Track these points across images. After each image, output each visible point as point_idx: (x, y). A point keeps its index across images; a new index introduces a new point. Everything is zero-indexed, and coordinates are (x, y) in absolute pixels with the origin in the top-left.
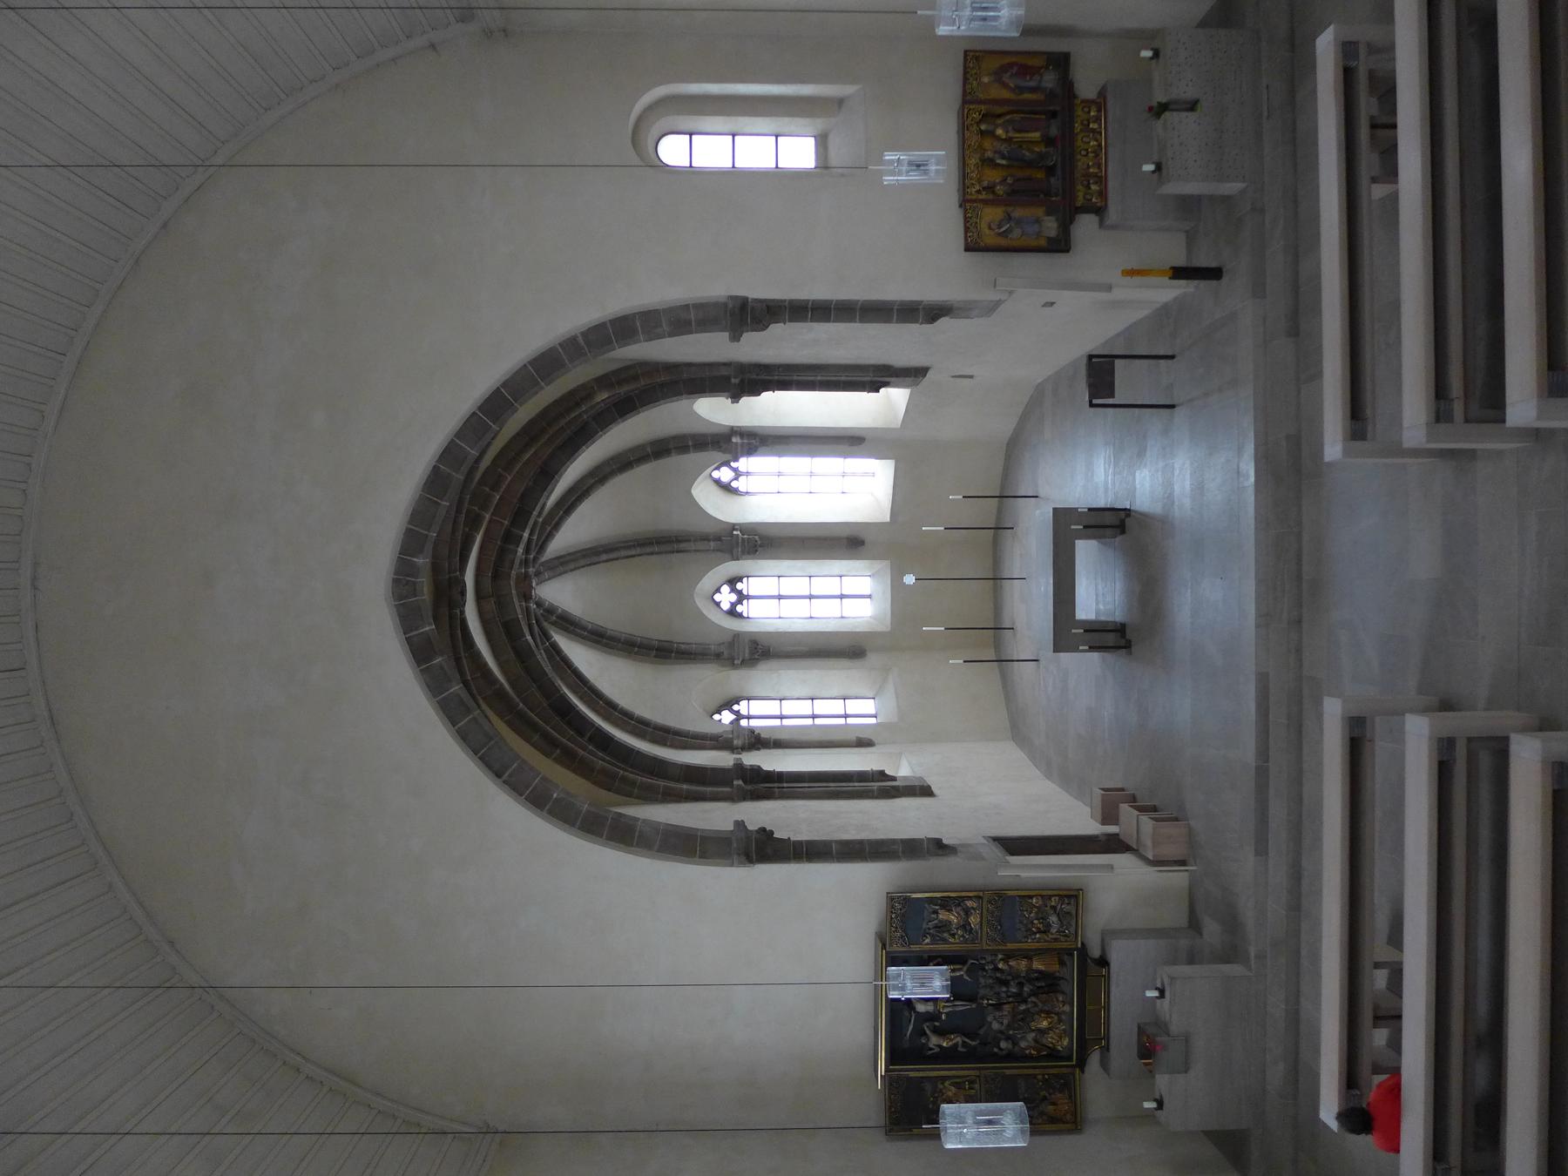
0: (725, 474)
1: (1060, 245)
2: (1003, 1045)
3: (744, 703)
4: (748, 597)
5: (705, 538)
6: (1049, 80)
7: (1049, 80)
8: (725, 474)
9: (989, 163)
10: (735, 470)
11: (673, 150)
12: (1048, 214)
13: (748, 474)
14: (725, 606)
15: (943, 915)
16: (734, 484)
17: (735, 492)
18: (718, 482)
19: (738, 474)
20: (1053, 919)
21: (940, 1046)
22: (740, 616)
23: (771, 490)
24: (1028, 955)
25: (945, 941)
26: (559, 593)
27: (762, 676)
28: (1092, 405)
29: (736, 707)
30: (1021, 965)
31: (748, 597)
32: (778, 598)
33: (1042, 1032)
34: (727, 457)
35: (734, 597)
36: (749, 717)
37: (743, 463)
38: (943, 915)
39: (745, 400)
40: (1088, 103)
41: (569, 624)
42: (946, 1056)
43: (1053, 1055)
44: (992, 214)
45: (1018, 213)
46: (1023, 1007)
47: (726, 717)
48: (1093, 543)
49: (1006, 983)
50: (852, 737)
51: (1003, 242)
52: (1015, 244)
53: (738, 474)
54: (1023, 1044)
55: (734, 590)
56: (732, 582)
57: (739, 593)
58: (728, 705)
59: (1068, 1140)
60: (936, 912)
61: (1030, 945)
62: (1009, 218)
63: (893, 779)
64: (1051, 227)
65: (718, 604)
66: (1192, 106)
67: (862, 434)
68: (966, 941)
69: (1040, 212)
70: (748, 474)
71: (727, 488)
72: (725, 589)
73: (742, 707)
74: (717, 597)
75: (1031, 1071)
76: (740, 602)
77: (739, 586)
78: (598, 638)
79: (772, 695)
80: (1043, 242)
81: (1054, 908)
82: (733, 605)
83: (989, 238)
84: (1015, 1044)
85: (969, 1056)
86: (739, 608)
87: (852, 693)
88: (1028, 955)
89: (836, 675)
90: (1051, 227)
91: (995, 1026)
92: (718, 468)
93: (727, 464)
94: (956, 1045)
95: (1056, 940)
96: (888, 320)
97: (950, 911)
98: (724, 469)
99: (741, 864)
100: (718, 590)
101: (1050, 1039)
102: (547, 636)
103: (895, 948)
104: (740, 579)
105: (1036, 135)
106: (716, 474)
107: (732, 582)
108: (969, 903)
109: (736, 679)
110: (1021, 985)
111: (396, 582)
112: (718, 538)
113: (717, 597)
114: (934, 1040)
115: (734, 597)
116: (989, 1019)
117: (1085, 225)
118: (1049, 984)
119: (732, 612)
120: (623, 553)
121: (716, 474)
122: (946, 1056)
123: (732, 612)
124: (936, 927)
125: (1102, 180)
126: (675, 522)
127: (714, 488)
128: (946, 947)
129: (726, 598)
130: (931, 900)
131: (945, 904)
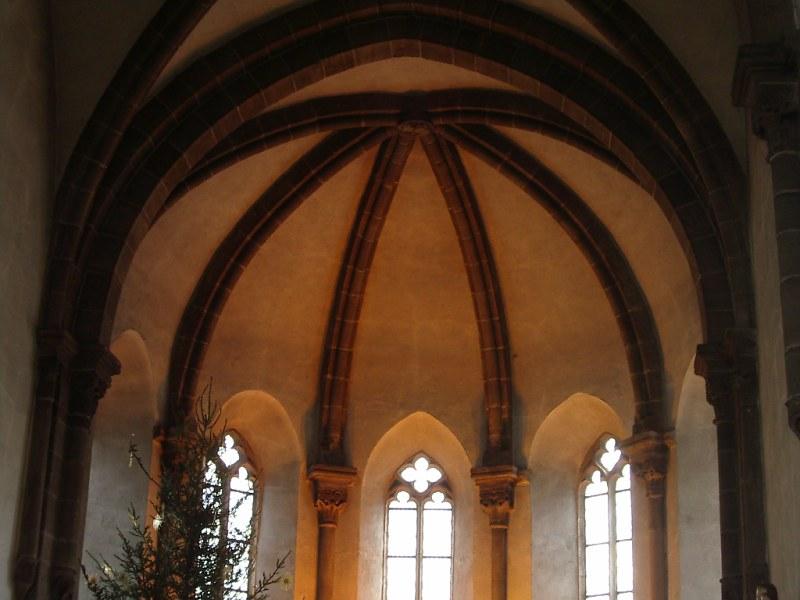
0: (611, 456)
4: (420, 510)
8: (611, 456)
14: (407, 475)
16: (596, 475)
17: (584, 477)
19: (611, 477)
26: (418, 212)
29: (243, 472)
31: (420, 510)
35: (421, 487)
39: (720, 585)
41: (373, 204)
48: (403, 177)
55: (433, 487)
56: (445, 485)
64: (713, 398)
65: (410, 461)
71: (591, 459)
72: (436, 475)
74: (422, 463)
77: (438, 497)
78: (357, 253)
86: (403, 496)
93: (625, 458)
100: (433, 462)
102: (322, 124)
104: (449, 497)
107: (445, 485)
113: (422, 463)
115: (421, 487)
123: (395, 485)
126: (528, 380)
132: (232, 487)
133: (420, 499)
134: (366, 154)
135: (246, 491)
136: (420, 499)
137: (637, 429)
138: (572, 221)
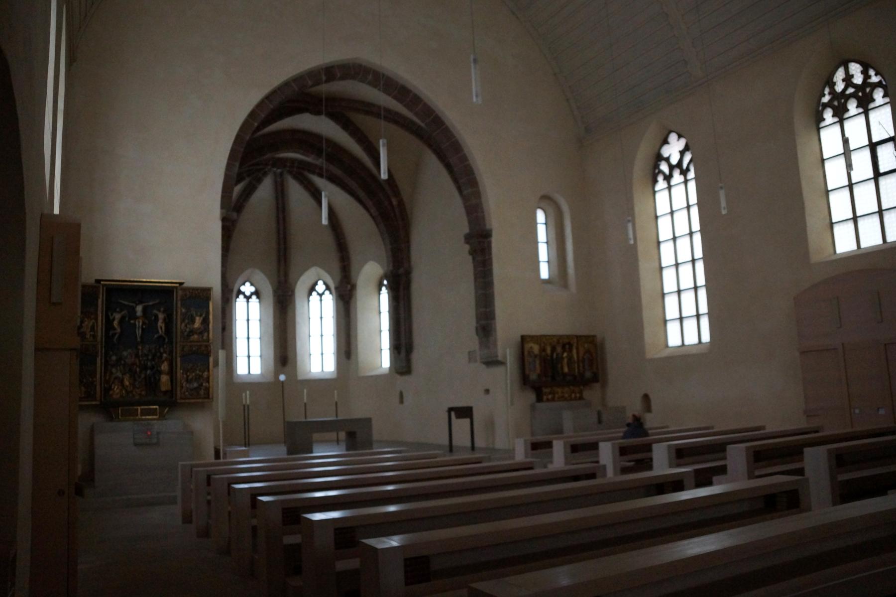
0: (320, 287)
1: (525, 380)
2: (114, 358)
4: (248, 302)
5: (286, 275)
6: (588, 374)
7: (588, 374)
8: (320, 287)
9: (554, 349)
10: (323, 293)
11: (541, 216)
12: (539, 376)
14: (243, 288)
15: (198, 321)
16: (314, 293)
17: (310, 294)
18: (316, 284)
20: (195, 385)
21: (114, 319)
22: (237, 297)
23: (318, 313)
24: (171, 373)
25: (183, 321)
28: (450, 410)
30: (165, 367)
31: (248, 302)
32: (318, 313)
33: (122, 382)
34: (332, 286)
35: (248, 294)
37: (329, 300)
38: (198, 321)
40: (581, 392)
42: (109, 322)
43: (107, 390)
44: (536, 349)
45: (538, 362)
46: (138, 370)
49: (153, 359)
51: (526, 353)
52: (526, 358)
53: (321, 295)
54: (114, 370)
55: (252, 294)
56: (257, 293)
57: (250, 297)
60: (201, 316)
61: (180, 372)
62: (536, 356)
64: (349, 286)
65: (244, 284)
66: (600, 422)
67: (353, 357)
68: (182, 332)
69: (538, 371)
71: (312, 289)
72: (253, 289)
74: (248, 284)
75: (98, 376)
76: (245, 297)
77: (254, 297)
80: (527, 372)
81: (201, 385)
82: (243, 293)
83: (528, 346)
84: (113, 366)
85: (108, 337)
86: (241, 296)
88: (171, 373)
90: (533, 376)
91: (125, 353)
92: (325, 283)
94: (115, 329)
95: (182, 387)
96: (478, 305)
97: (202, 323)
98: (324, 287)
99: (222, 214)
100: (252, 284)
101: (116, 388)
103: (180, 293)
104: (258, 297)
105: (566, 370)
106: (320, 283)
107: (257, 293)
108: (206, 334)
110: (152, 368)
111: (360, 66)
112: (286, 281)
113: (248, 284)
114: (118, 316)
115: (248, 294)
116: (130, 351)
117: (532, 397)
118: (152, 384)
119: (240, 292)
120: (281, 216)
121: (320, 283)
122: (109, 322)
124: (192, 316)
125: (553, 400)
126: (355, 258)
128: (179, 323)
129: (248, 289)
130: (208, 313)
131: (206, 321)
132: (320, 370)
133: (248, 298)
134: (406, 536)
135: (454, 443)
136: (248, 298)
138: (189, 403)
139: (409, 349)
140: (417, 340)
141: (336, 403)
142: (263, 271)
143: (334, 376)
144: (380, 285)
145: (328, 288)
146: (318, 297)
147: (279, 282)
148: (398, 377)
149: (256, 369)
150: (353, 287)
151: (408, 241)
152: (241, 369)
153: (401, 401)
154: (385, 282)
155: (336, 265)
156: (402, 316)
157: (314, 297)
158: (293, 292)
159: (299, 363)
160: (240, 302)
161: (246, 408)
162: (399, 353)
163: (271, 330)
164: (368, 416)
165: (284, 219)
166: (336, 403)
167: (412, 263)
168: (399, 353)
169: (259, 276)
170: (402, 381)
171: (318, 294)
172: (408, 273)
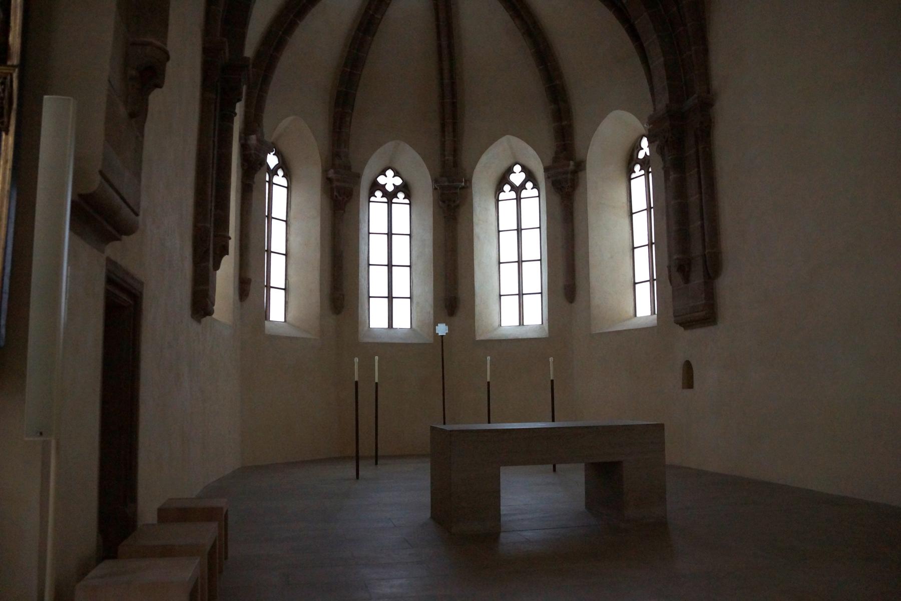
0: (518, 177)
3: (284, 182)
4: (390, 203)
5: (456, 152)
8: (518, 177)
10: (523, 186)
13: (518, 199)
14: (381, 180)
16: (507, 188)
17: (500, 189)
18: (510, 171)
19: (518, 190)
23: (514, 231)
27: (312, 198)
31: (390, 203)
32: (514, 231)
35: (390, 188)
36: (271, 183)
37: (533, 206)
47: (272, 160)
50: (252, 275)
53: (518, 190)
55: (397, 189)
56: (405, 188)
58: (283, 164)
59: (712, 328)
63: (217, 266)
65: (383, 173)
70: (518, 199)
71: (504, 179)
72: (398, 181)
73: (280, 179)
74: (390, 173)
76: (385, 194)
77: (401, 195)
79: (292, 214)
82: (382, 188)
86: (378, 194)
87: (291, 261)
89: (312, 279)
92: (524, 169)
98: (523, 176)
100: (397, 174)
106: (517, 168)
107: (405, 188)
109: (312, 173)
112: (456, 164)
113: (390, 173)
115: (390, 188)
119: (375, 186)
120: (444, 43)
121: (517, 168)
126: (581, 110)
127: (505, 165)
133: (390, 197)
136: (390, 197)
137: (556, 159)
139: (713, 267)
140: (729, 242)
141: (552, 381)
142: (414, 146)
143: (544, 334)
144: (631, 161)
145: (530, 176)
146: (513, 195)
147: (444, 164)
148: (681, 330)
149: (403, 320)
150: (580, 166)
151: (702, 37)
152: (377, 318)
153: (688, 382)
154: (645, 149)
155: (545, 128)
156: (693, 199)
157: (507, 193)
158: (469, 181)
159: (478, 309)
160: (377, 210)
161: (357, 383)
162: (687, 279)
163: (429, 250)
164: (696, 385)
165: (451, 46)
166: (552, 381)
167: (715, 83)
168: (687, 279)
169: (411, 157)
170: (688, 343)
171: (513, 188)
172: (707, 104)
